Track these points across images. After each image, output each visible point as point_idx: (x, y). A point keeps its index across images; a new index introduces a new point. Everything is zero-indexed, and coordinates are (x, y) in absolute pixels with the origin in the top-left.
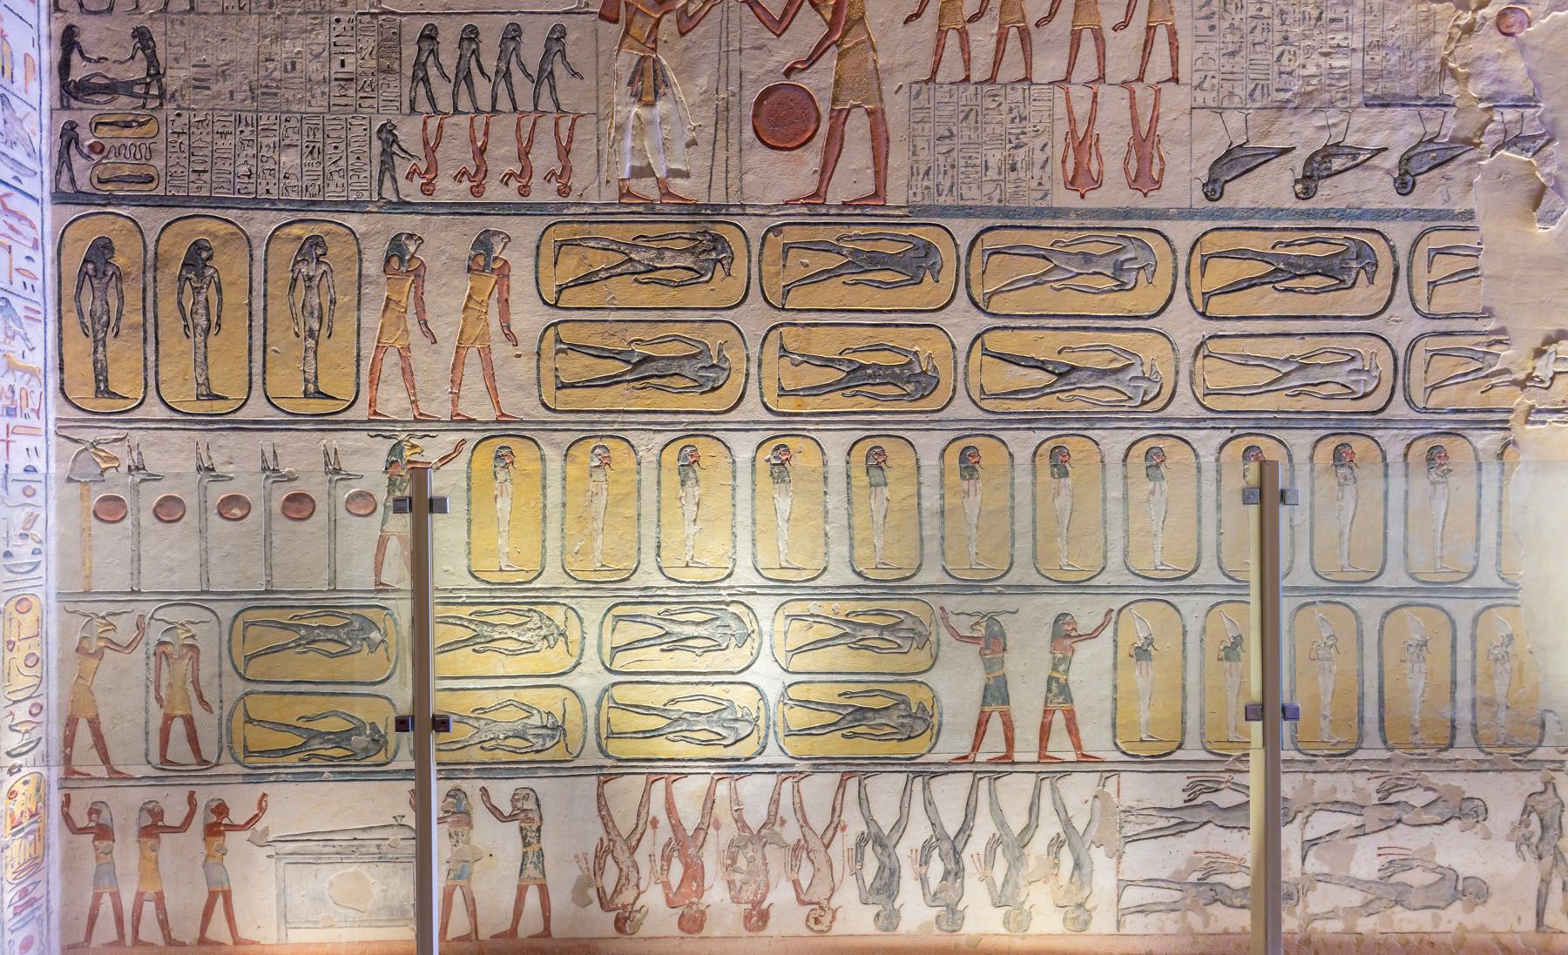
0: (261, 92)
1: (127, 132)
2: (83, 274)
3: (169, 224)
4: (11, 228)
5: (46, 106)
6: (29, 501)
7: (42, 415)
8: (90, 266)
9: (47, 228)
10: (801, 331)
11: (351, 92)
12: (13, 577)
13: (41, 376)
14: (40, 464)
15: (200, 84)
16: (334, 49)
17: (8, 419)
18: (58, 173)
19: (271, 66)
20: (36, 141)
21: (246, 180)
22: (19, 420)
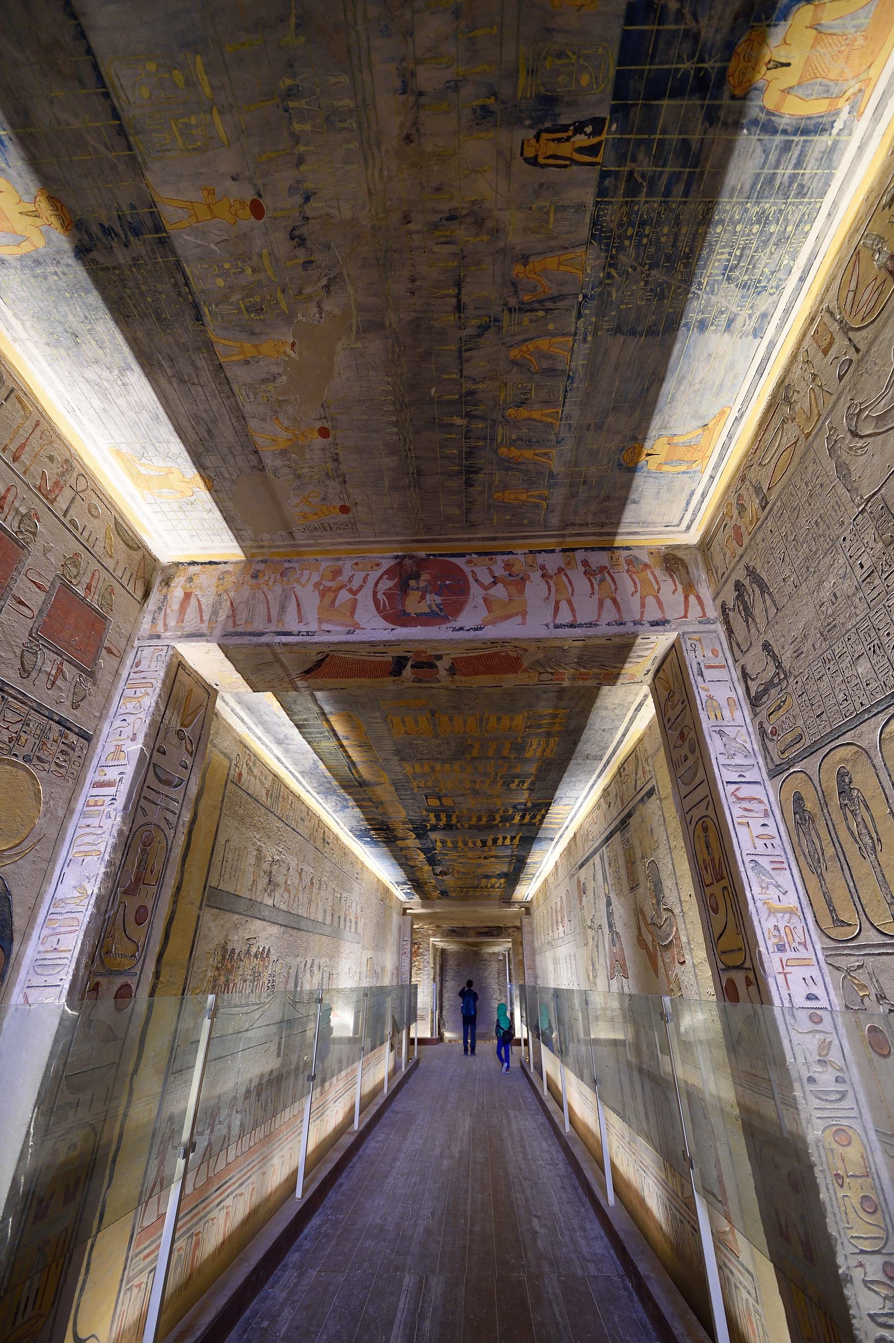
0: (828, 631)
1: (781, 712)
2: (797, 823)
3: (820, 765)
4: (745, 809)
5: (748, 720)
6: (818, 1027)
7: (810, 946)
8: (797, 816)
9: (772, 798)
10: (222, 791)
11: (877, 582)
12: (823, 1104)
13: (800, 913)
14: (819, 991)
15: (798, 653)
16: (851, 561)
17: (780, 954)
18: (766, 758)
19: (824, 608)
20: (748, 746)
21: (846, 703)
22: (789, 954)
